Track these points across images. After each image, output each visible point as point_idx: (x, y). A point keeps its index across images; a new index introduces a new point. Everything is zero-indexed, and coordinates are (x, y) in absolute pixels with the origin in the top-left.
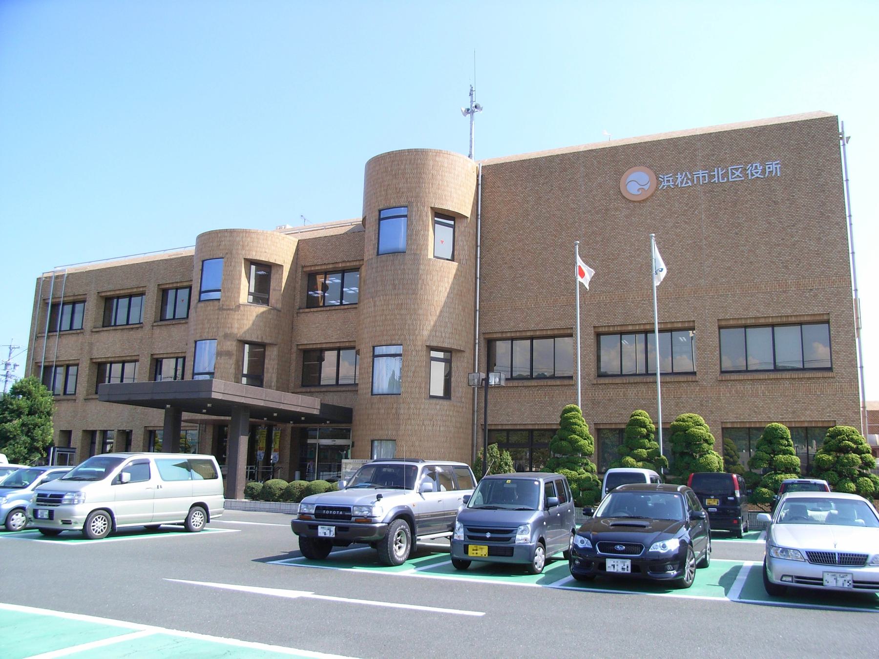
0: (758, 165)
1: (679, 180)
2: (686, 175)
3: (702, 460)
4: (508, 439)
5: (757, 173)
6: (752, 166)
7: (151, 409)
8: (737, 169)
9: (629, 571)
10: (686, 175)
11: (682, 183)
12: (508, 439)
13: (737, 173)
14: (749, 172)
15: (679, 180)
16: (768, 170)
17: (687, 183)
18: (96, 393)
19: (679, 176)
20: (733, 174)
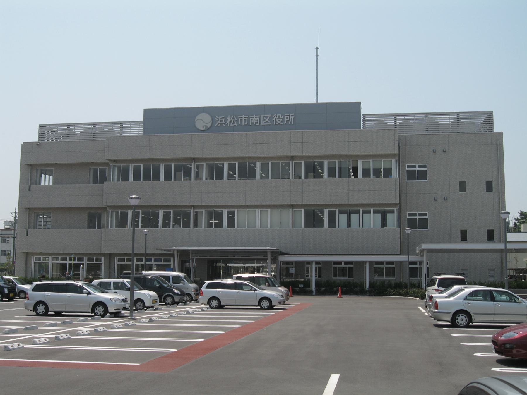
0: (280, 115)
1: (229, 121)
2: (233, 118)
3: (386, 283)
4: (121, 133)
5: (279, 120)
6: (276, 115)
7: (323, 203)
8: (267, 117)
9: (51, 183)
10: (233, 118)
11: (230, 123)
12: (121, 133)
13: (267, 120)
14: (274, 119)
15: (229, 121)
16: (286, 119)
17: (234, 123)
18: (146, 235)
19: (229, 118)
20: (264, 120)
